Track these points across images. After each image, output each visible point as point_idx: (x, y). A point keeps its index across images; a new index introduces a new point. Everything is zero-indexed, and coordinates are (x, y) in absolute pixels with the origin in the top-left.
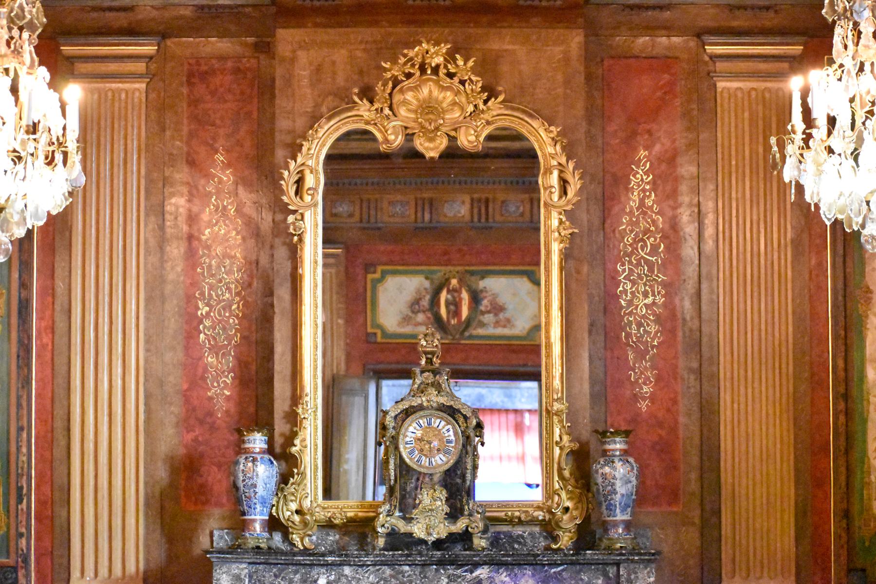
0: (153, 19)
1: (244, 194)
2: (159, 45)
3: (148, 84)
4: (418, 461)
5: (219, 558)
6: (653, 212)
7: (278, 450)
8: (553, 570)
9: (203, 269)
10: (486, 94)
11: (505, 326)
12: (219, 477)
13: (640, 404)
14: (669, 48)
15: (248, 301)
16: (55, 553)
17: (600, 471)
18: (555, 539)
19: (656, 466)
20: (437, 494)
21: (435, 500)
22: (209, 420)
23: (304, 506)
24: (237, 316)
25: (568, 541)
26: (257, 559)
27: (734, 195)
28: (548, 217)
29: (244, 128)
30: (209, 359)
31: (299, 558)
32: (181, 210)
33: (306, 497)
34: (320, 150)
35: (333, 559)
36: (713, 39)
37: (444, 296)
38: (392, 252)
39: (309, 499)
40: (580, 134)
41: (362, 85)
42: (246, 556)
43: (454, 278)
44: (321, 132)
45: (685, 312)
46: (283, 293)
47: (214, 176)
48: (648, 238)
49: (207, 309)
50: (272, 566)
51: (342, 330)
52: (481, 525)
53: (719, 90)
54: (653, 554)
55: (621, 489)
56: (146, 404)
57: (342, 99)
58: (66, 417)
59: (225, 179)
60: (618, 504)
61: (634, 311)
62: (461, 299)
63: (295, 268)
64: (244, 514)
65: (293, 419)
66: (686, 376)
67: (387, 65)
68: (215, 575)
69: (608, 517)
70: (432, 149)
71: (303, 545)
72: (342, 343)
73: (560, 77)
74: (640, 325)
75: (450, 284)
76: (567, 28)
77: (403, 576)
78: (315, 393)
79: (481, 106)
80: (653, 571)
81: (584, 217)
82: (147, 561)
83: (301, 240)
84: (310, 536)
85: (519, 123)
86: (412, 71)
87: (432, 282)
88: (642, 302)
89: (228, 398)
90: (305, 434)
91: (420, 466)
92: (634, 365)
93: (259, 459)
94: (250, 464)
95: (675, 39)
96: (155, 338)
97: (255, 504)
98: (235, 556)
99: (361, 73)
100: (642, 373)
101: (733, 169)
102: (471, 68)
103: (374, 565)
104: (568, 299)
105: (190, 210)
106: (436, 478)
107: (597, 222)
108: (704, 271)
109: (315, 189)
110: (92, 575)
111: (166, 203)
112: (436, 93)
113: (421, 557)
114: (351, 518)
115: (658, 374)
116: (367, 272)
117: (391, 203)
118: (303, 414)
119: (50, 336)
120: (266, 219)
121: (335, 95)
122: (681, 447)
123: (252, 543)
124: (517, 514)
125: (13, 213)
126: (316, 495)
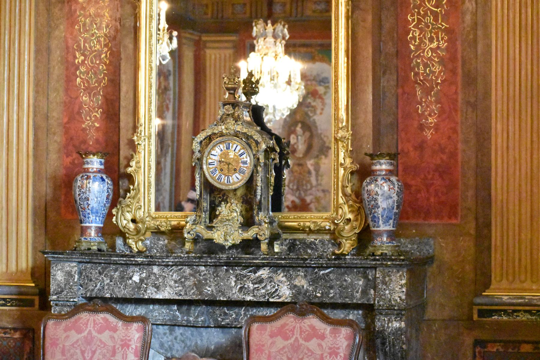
5: (54, 257)
8: (322, 272)
13: (426, 133)
15: (114, 52)
17: (366, 188)
18: (339, 245)
21: (232, 212)
23: (138, 216)
24: (105, 64)
25: (349, 248)
26: (82, 258)
30: (84, 98)
31: (115, 259)
35: (142, 259)
49: (83, 58)
50: (97, 265)
55: (383, 204)
60: (380, 216)
61: (422, 54)
69: (374, 227)
74: (426, 66)
77: (200, 275)
80: (405, 274)
82: (34, 259)
84: (142, 240)
89: (97, 129)
90: (139, 158)
92: (421, 99)
93: (92, 178)
96: (42, 82)
98: (66, 256)
100: (428, 107)
113: (211, 259)
114: (174, 225)
115: (442, 107)
118: (138, 140)
122: (460, 169)
123: (84, 246)
124: (308, 224)
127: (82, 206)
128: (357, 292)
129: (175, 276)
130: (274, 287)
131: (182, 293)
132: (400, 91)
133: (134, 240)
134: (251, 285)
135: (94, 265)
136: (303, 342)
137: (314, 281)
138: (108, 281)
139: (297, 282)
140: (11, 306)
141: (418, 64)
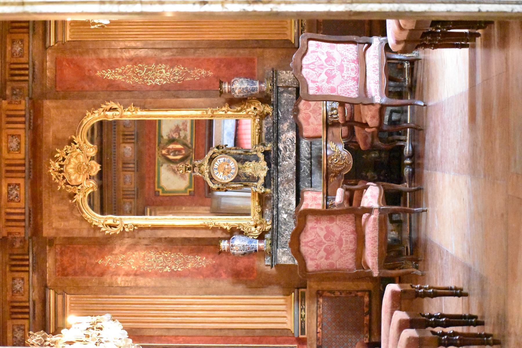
0: (39, 291)
1: (116, 251)
2: (50, 289)
3: (67, 294)
4: (233, 174)
5: (275, 261)
6: (124, 69)
7: (229, 236)
8: (280, 115)
9: (149, 269)
10: (72, 143)
11: (186, 125)
12: (242, 262)
14: (52, 62)
16: (276, 335)
17: (237, 94)
18: (268, 114)
19: (238, 68)
20: (247, 166)
22: (216, 267)
24: (170, 254)
27: (117, 33)
28: (126, 116)
29: (87, 251)
30: (189, 266)
32: (123, 279)
34: (96, 217)
36: (48, 43)
37: (171, 157)
38: (149, 183)
39: (250, 222)
40: (90, 102)
41: (68, 198)
43: (162, 152)
44: (89, 216)
45: (169, 55)
46: (160, 233)
47: (108, 264)
48: (136, 71)
49: (167, 267)
51: (188, 208)
52: (261, 147)
53: (70, 40)
54: (273, 71)
55: (245, 85)
56: (210, 294)
57: (74, 208)
58: (215, 331)
59: (109, 259)
60: (251, 87)
62: (173, 148)
63: (149, 228)
64: (256, 251)
65: (215, 229)
66: (197, 55)
67: (59, 188)
68: (282, 263)
70: (96, 167)
72: (195, 208)
73: (64, 111)
74: (174, 75)
75: (165, 154)
76: (43, 107)
77: (283, 181)
78: (204, 219)
79: (77, 146)
81: (126, 101)
82: (279, 294)
83: (136, 226)
84: (266, 222)
85: (85, 129)
86: (62, 176)
87: (164, 163)
88: (164, 74)
89: (207, 258)
91: (235, 173)
92: (192, 78)
94: (234, 248)
95: (48, 58)
99: (63, 199)
101: (105, 33)
102: (60, 150)
103: (278, 193)
104: (163, 107)
105: (124, 275)
106: (241, 166)
107: (128, 94)
108: (150, 47)
109: (114, 219)
110: (285, 319)
111: (120, 286)
112: (71, 166)
114: (258, 204)
116: (159, 195)
117: (125, 183)
119: (179, 337)
120: (128, 241)
121: (72, 210)
123: (269, 247)
124: (257, 131)
125: (122, 344)
126: (248, 219)
128: (290, 97)
129: (284, 194)
130: (288, 141)
131: (292, 190)
132: (188, 89)
134: (288, 153)
135: (278, 240)
136: (311, 108)
137: (285, 119)
138: (287, 232)
139: (286, 129)
140: (305, 305)
141: (174, 79)
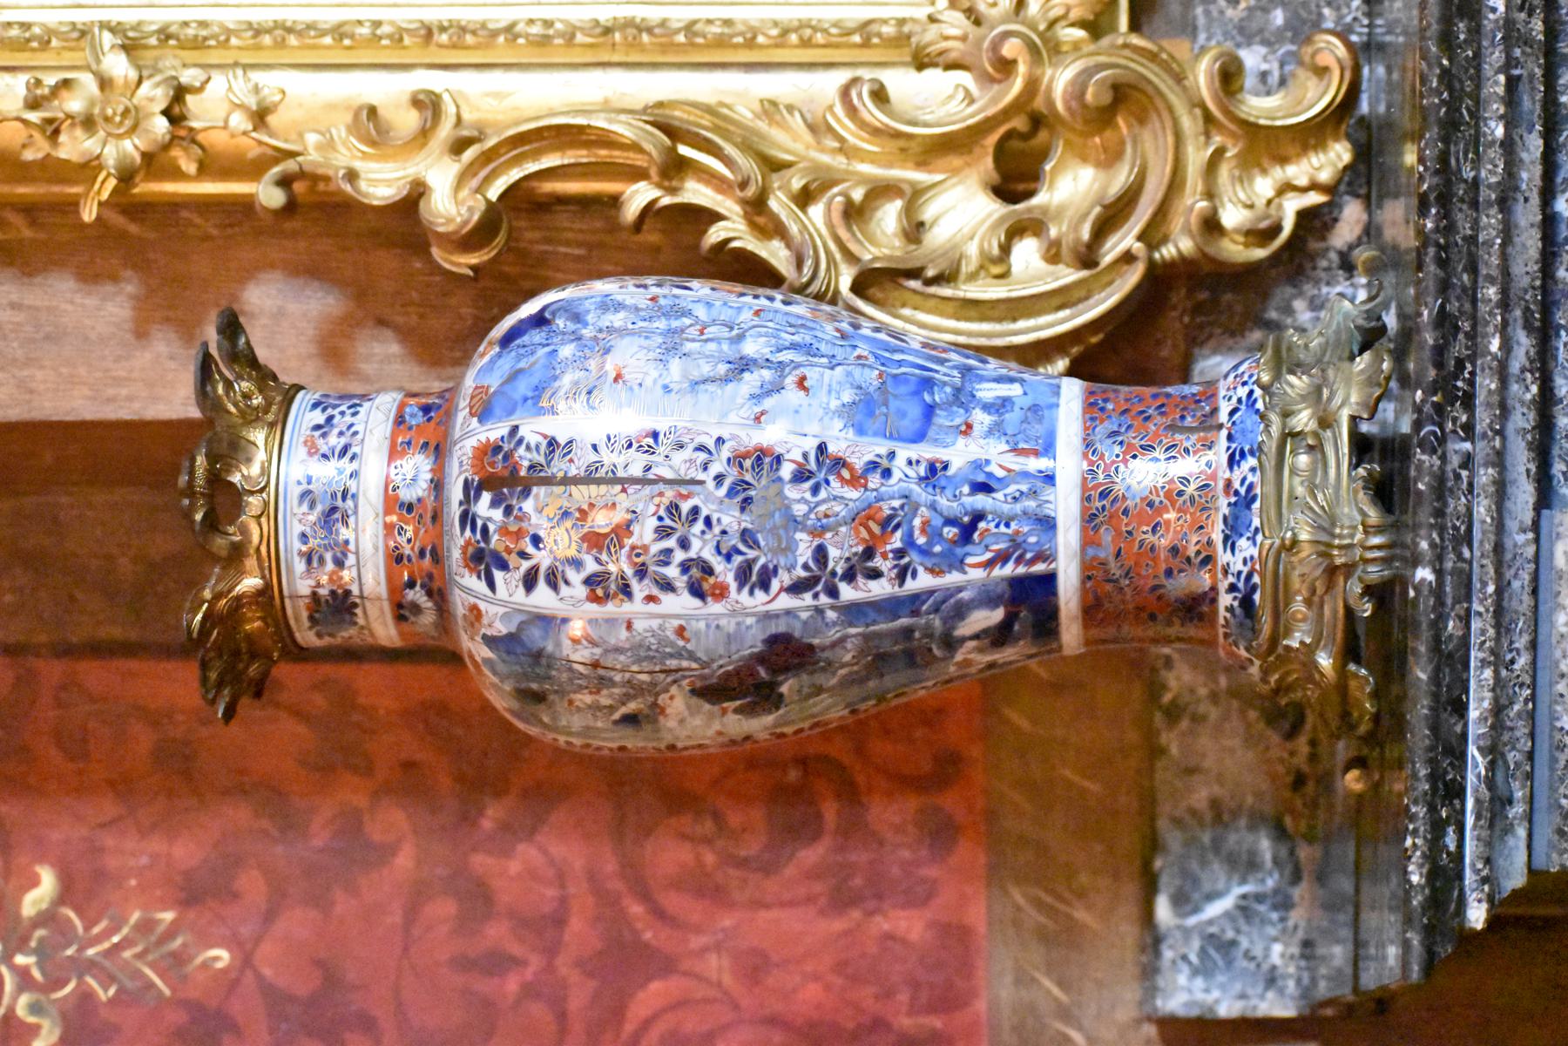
5: (1496, 807)
12: (716, 966)
33: (880, 95)
42: (1482, 510)
71: (1310, 135)
93: (495, 431)
97: (935, 471)
118: (134, 120)
127: (836, 556)
133: (1224, 172)
